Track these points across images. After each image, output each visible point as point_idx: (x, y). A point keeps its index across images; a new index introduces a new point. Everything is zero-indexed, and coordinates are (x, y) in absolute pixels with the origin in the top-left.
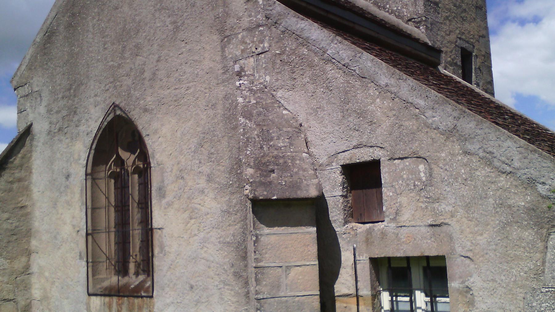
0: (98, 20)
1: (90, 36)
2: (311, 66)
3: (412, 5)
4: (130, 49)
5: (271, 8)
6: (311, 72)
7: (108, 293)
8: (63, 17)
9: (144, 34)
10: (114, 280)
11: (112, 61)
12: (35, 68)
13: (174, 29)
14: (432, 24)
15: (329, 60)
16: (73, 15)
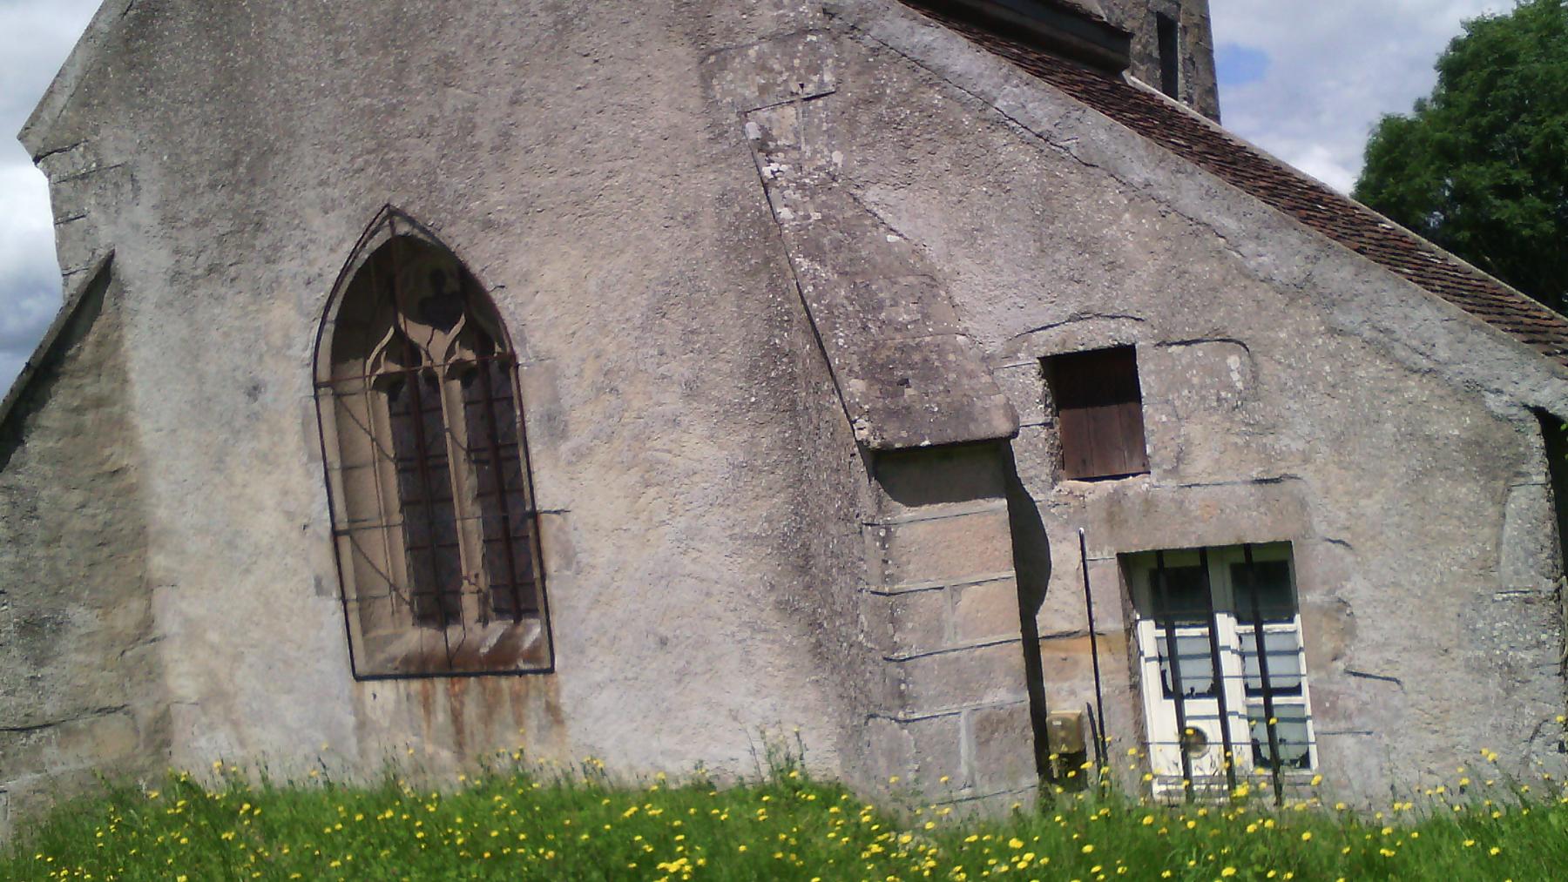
1: (284, 25)
2: (954, 133)
15: (1002, 122)
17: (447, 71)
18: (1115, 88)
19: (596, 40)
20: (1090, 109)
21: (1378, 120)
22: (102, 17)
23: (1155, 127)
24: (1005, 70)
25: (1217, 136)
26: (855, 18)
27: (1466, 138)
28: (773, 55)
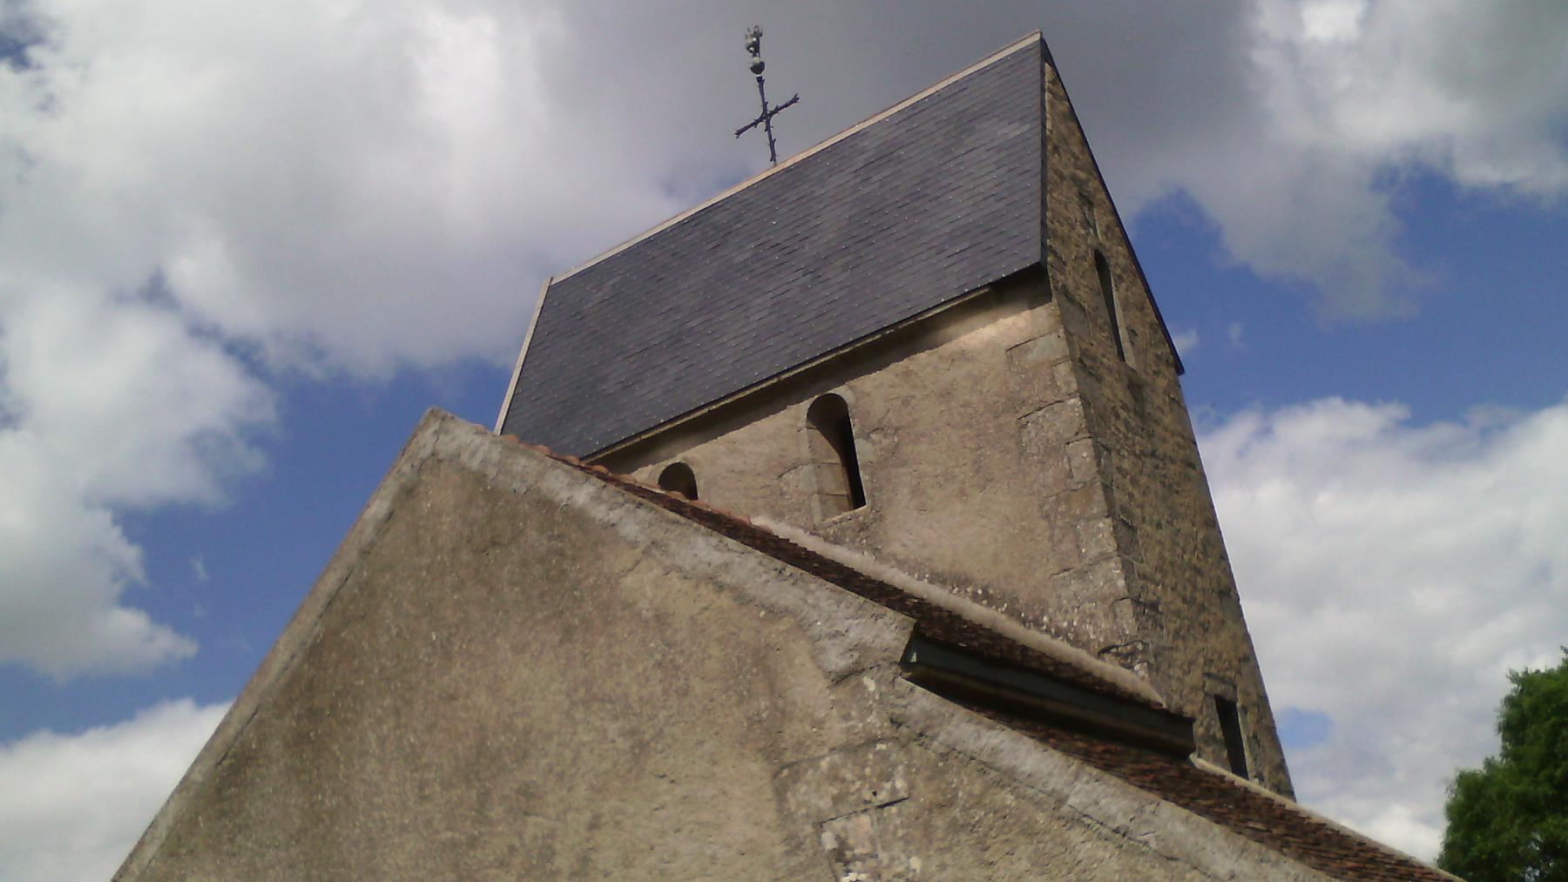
0: (398, 726)
1: (372, 765)
2: (1030, 832)
3: (1106, 616)
4: (504, 798)
5: (904, 702)
6: (1031, 848)
8: (280, 716)
9: (544, 762)
11: (449, 828)
12: (191, 852)
13: (632, 748)
14: (1156, 656)
15: (1077, 819)
16: (313, 714)
17: (529, 798)
18: (1183, 774)
19: (672, 761)
20: (1163, 803)
21: (1453, 776)
22: (198, 768)
23: (1230, 812)
24: (1073, 768)
25: (1294, 814)
26: (922, 725)
27: (1545, 789)
28: (844, 765)
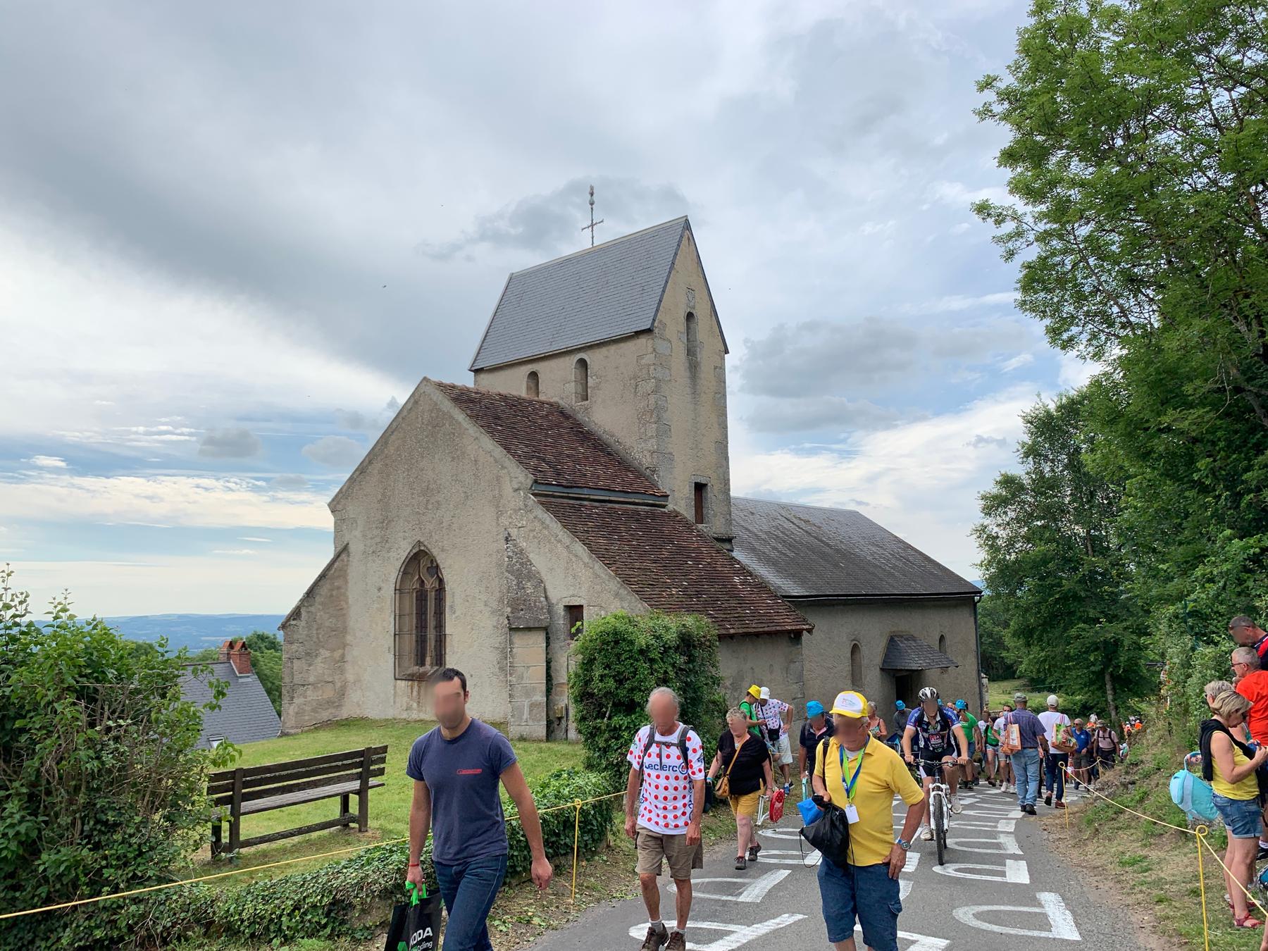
2: (549, 541)
7: (411, 678)
10: (416, 669)
